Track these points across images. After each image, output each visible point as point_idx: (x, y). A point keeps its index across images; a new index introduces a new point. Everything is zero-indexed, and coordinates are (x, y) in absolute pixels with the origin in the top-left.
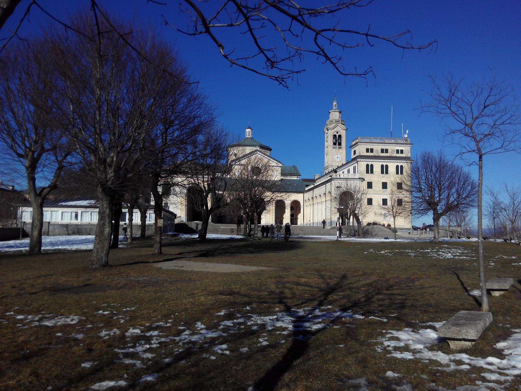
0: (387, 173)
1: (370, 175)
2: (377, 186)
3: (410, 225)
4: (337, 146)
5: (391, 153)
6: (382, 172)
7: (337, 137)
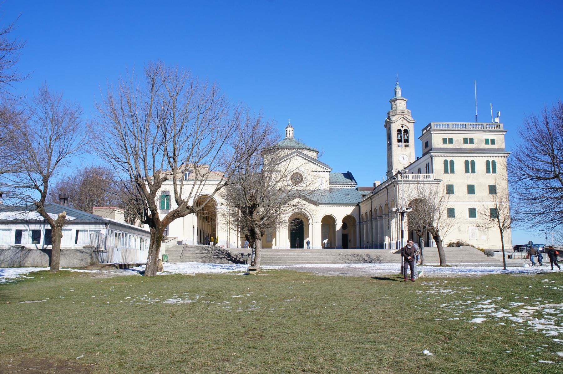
0: (473, 171)
1: (449, 175)
2: (460, 190)
3: (508, 245)
4: (404, 144)
5: (477, 143)
6: (467, 171)
7: (403, 132)
